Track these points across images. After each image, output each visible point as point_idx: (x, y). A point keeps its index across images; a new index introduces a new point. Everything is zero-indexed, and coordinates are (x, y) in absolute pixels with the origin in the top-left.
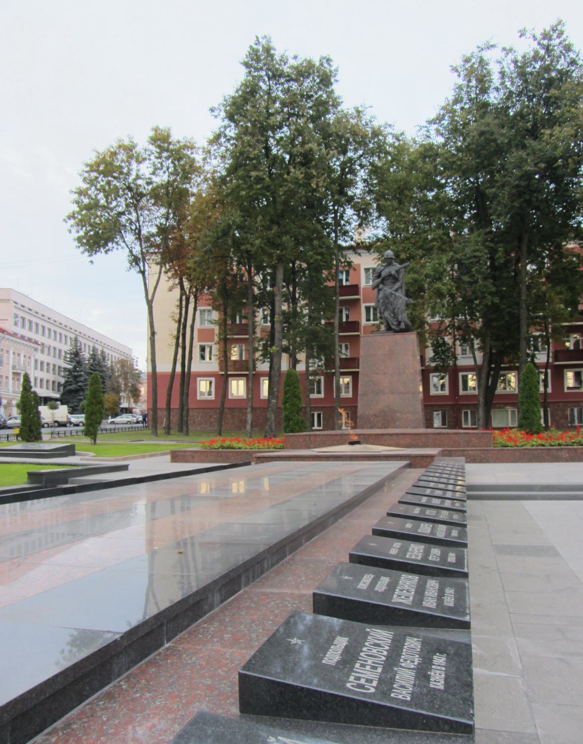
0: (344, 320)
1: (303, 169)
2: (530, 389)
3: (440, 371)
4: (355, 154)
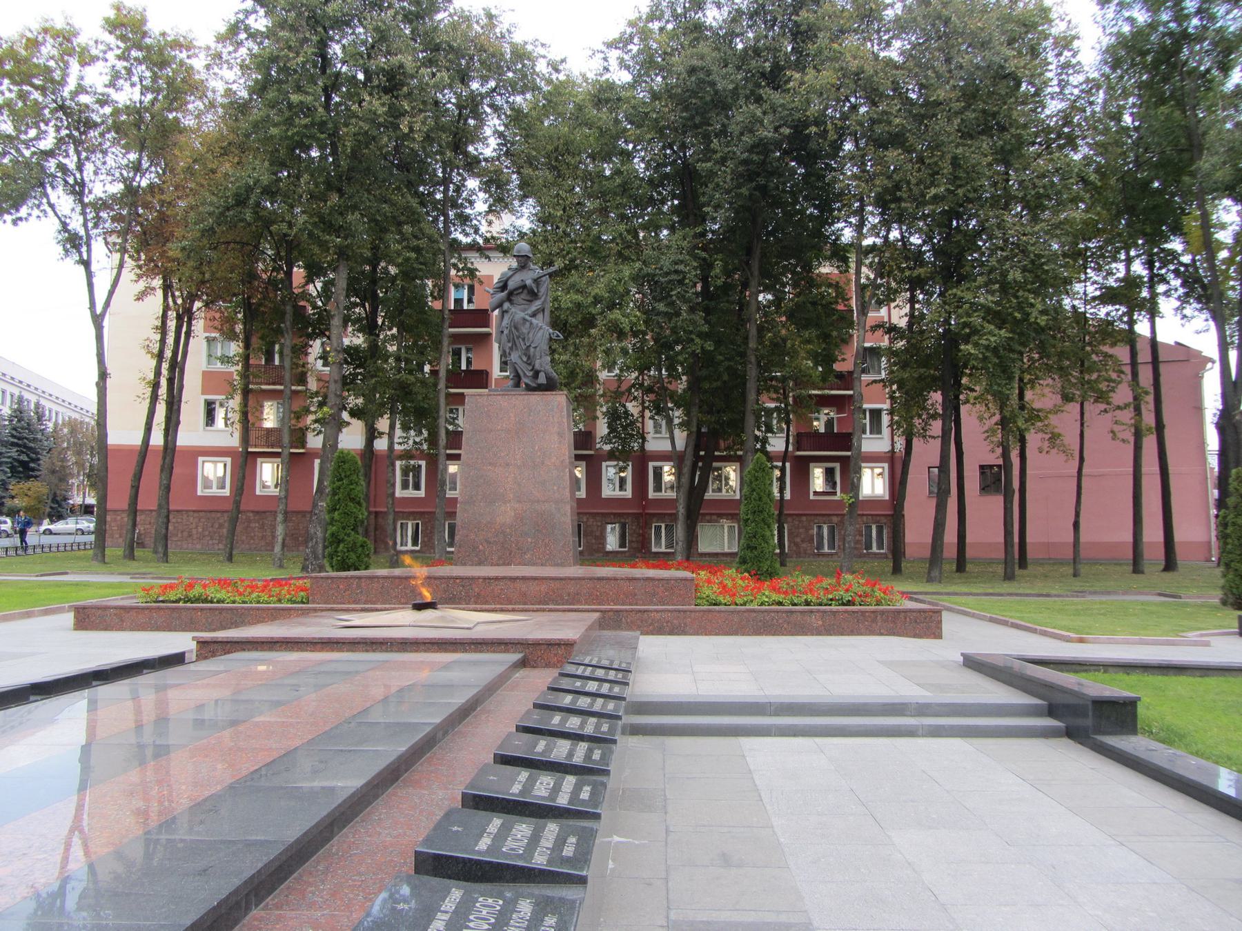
0: (464, 367)
1: (385, 98)
2: (760, 499)
3: (618, 459)
4: (482, 85)
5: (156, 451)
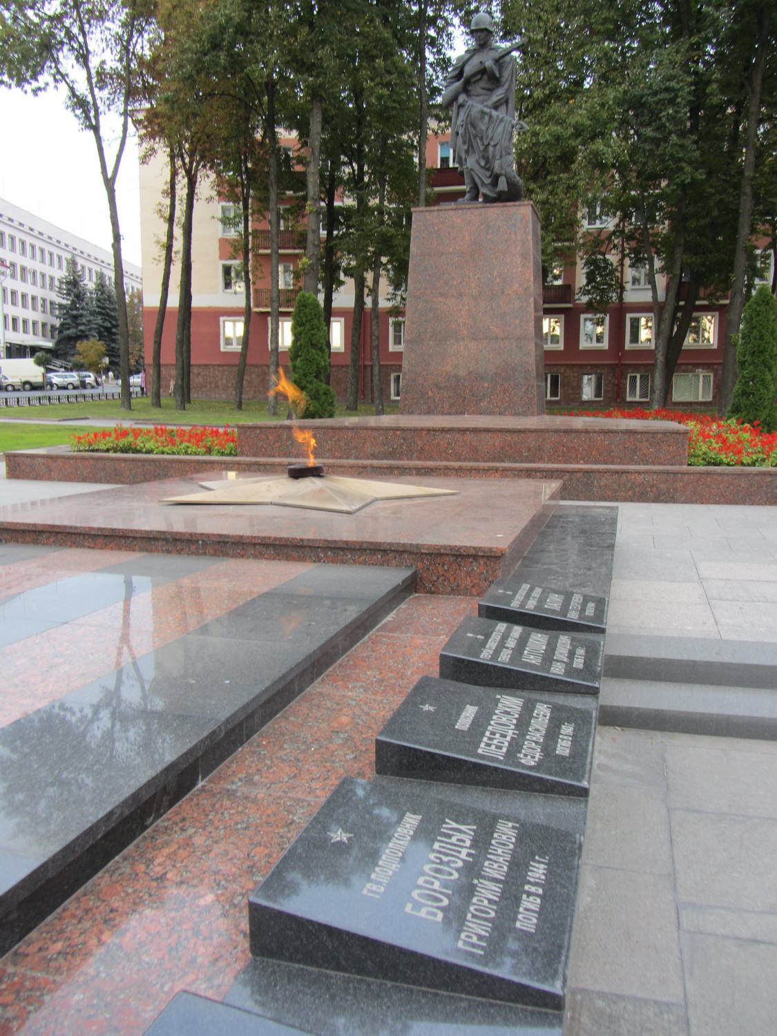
2: (762, 338)
5: (172, 311)
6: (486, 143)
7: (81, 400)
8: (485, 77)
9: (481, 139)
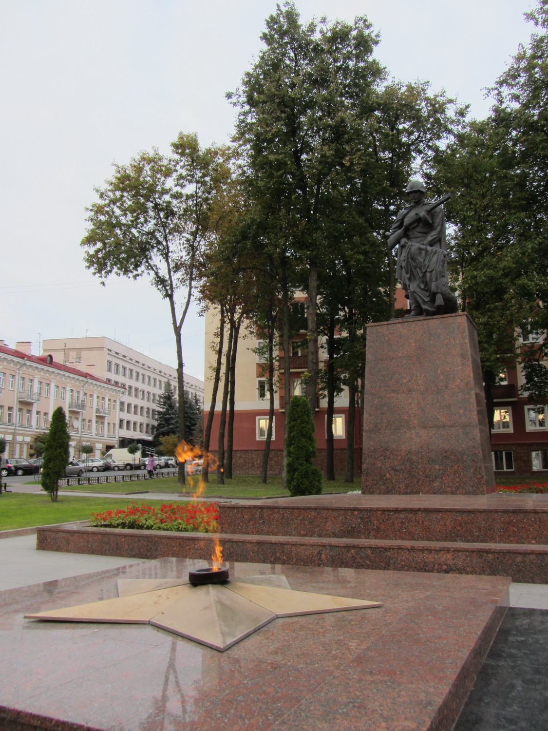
3: (536, 403)
6: (424, 271)
7: (135, 479)
8: (421, 224)
9: (420, 269)
